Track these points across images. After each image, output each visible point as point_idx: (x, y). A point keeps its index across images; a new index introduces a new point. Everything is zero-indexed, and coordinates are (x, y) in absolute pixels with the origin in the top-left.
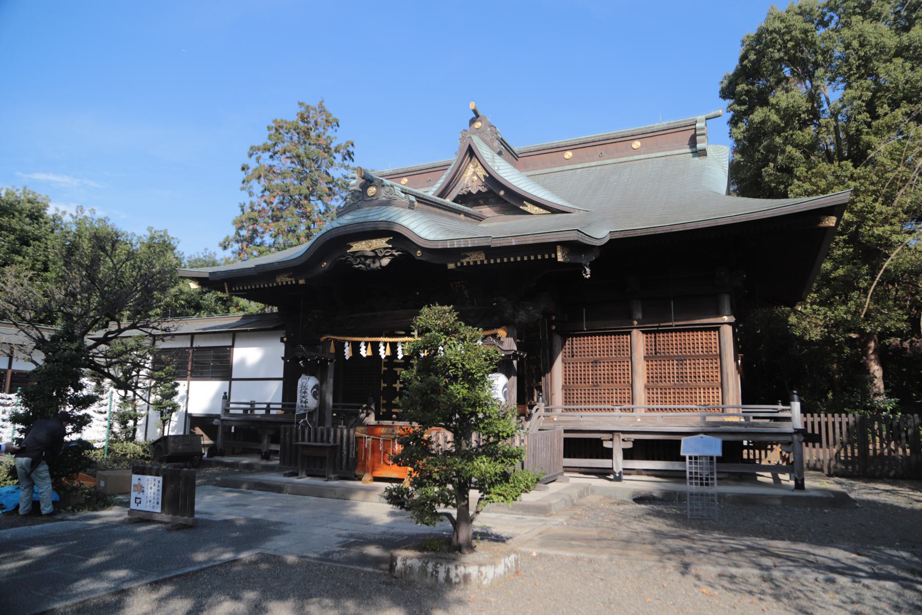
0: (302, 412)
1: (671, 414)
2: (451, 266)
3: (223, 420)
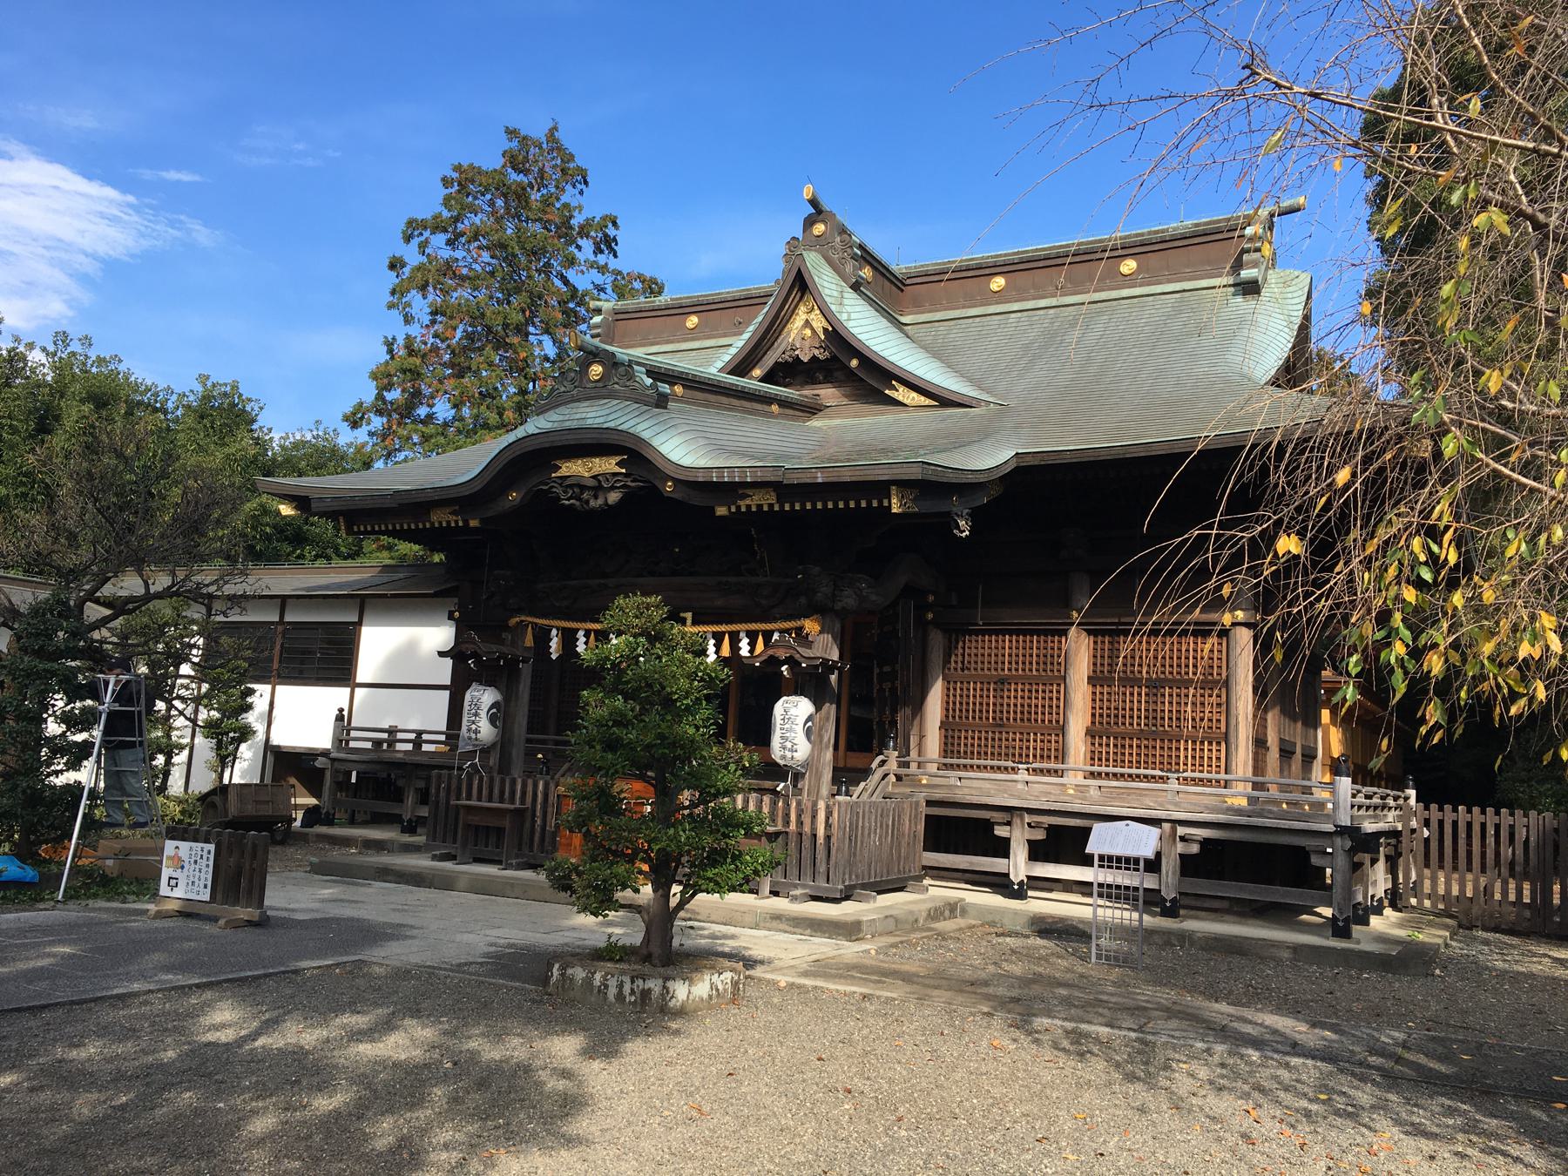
0: (470, 748)
1: (1115, 783)
2: (721, 511)
3: (334, 760)
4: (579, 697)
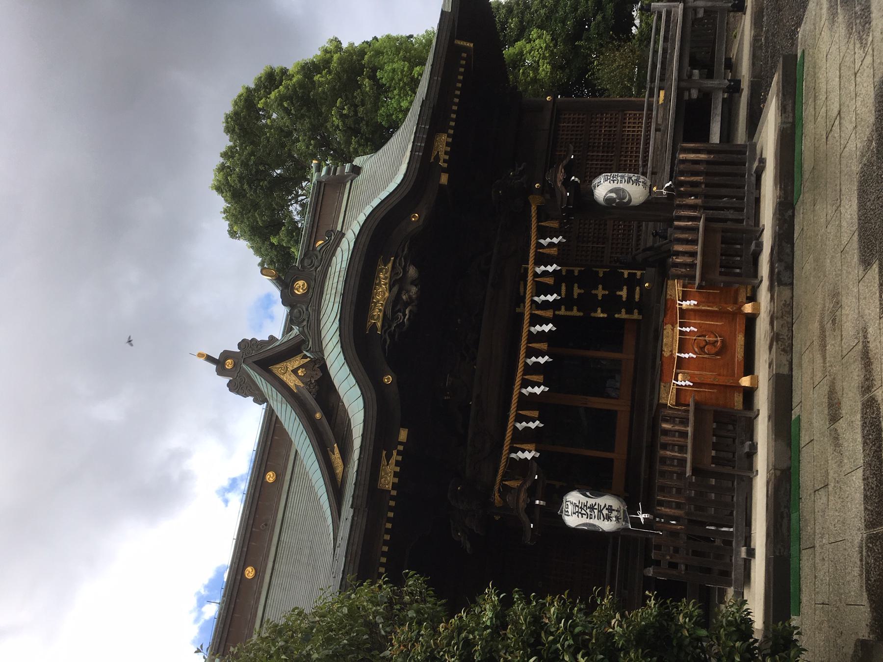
2: (444, 179)
4: (608, 200)
